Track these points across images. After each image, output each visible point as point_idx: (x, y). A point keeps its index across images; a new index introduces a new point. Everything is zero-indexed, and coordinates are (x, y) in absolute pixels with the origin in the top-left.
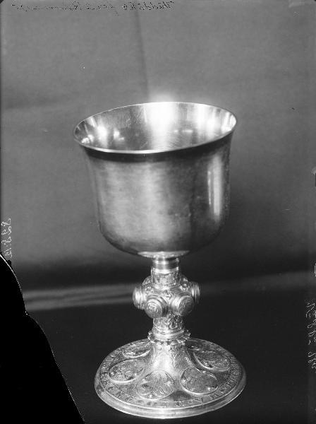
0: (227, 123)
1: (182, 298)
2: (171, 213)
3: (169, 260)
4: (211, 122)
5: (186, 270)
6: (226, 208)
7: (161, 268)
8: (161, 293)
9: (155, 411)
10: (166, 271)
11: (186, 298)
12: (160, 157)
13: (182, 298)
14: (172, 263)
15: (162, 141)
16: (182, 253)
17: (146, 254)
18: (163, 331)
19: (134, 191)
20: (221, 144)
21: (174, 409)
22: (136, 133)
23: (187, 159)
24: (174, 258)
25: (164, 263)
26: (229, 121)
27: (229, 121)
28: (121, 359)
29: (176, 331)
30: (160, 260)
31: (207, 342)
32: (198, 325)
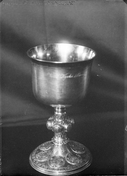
0: (92, 55)
1: (68, 125)
2: (67, 87)
3: (62, 108)
4: (84, 53)
5: (67, 114)
6: (62, 92)
7: (58, 112)
8: (56, 123)
9: (54, 172)
10: (60, 114)
11: (70, 125)
12: (63, 66)
13: (68, 125)
14: (63, 110)
15: (64, 58)
16: (67, 106)
17: (53, 106)
18: (58, 140)
19: (49, 80)
20: (87, 63)
21: (63, 171)
22: (55, 57)
23: (74, 66)
24: (64, 108)
25: (60, 110)
26: (92, 55)
27: (92, 55)
28: (39, 151)
29: (63, 138)
30: (58, 108)
31: (76, 142)
32: (72, 137)
